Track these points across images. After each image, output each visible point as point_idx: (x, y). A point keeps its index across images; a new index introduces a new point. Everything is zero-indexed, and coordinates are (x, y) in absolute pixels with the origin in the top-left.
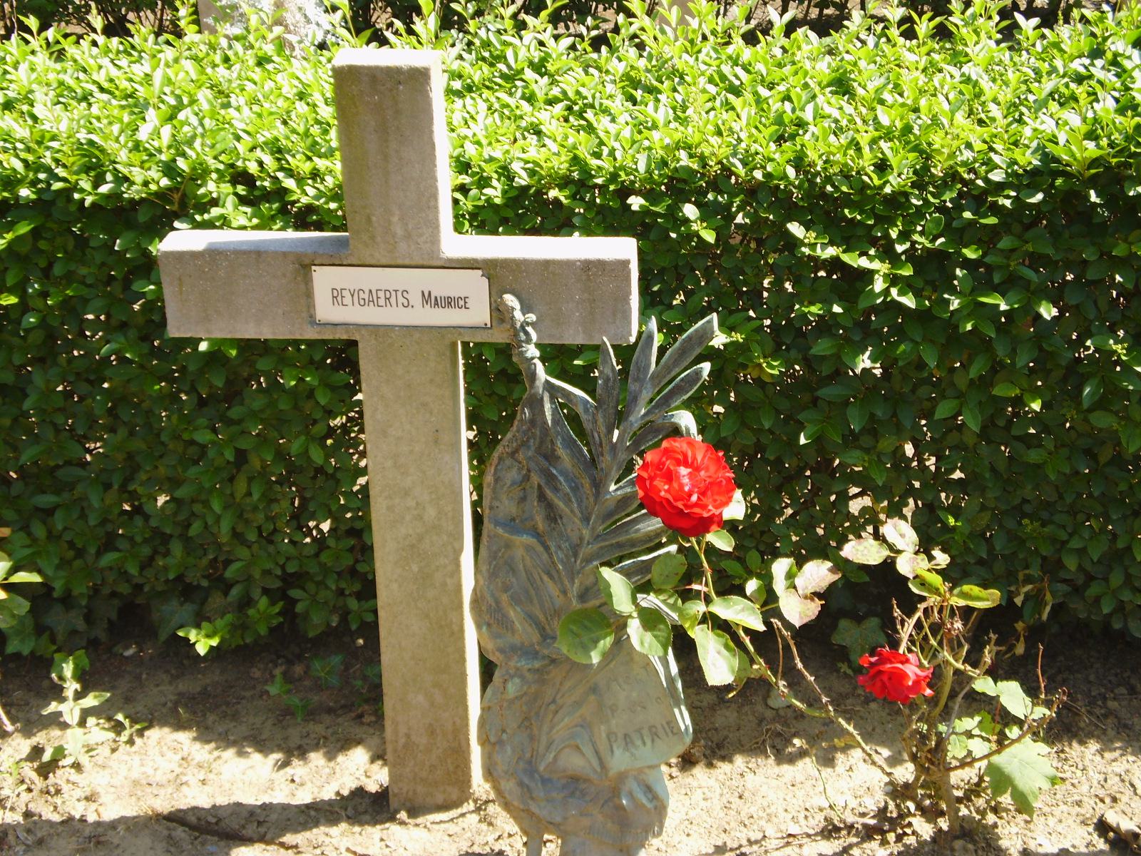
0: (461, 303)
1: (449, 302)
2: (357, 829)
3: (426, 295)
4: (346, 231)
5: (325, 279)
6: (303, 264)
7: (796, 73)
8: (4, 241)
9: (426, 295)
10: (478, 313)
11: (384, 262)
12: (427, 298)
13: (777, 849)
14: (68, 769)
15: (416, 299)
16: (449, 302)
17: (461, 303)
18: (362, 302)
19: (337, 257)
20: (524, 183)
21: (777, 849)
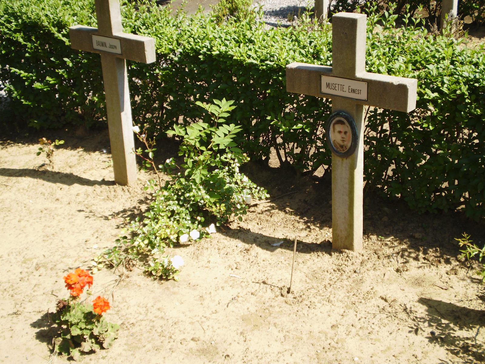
1: (353, 91)
15: (346, 88)
16: (353, 91)
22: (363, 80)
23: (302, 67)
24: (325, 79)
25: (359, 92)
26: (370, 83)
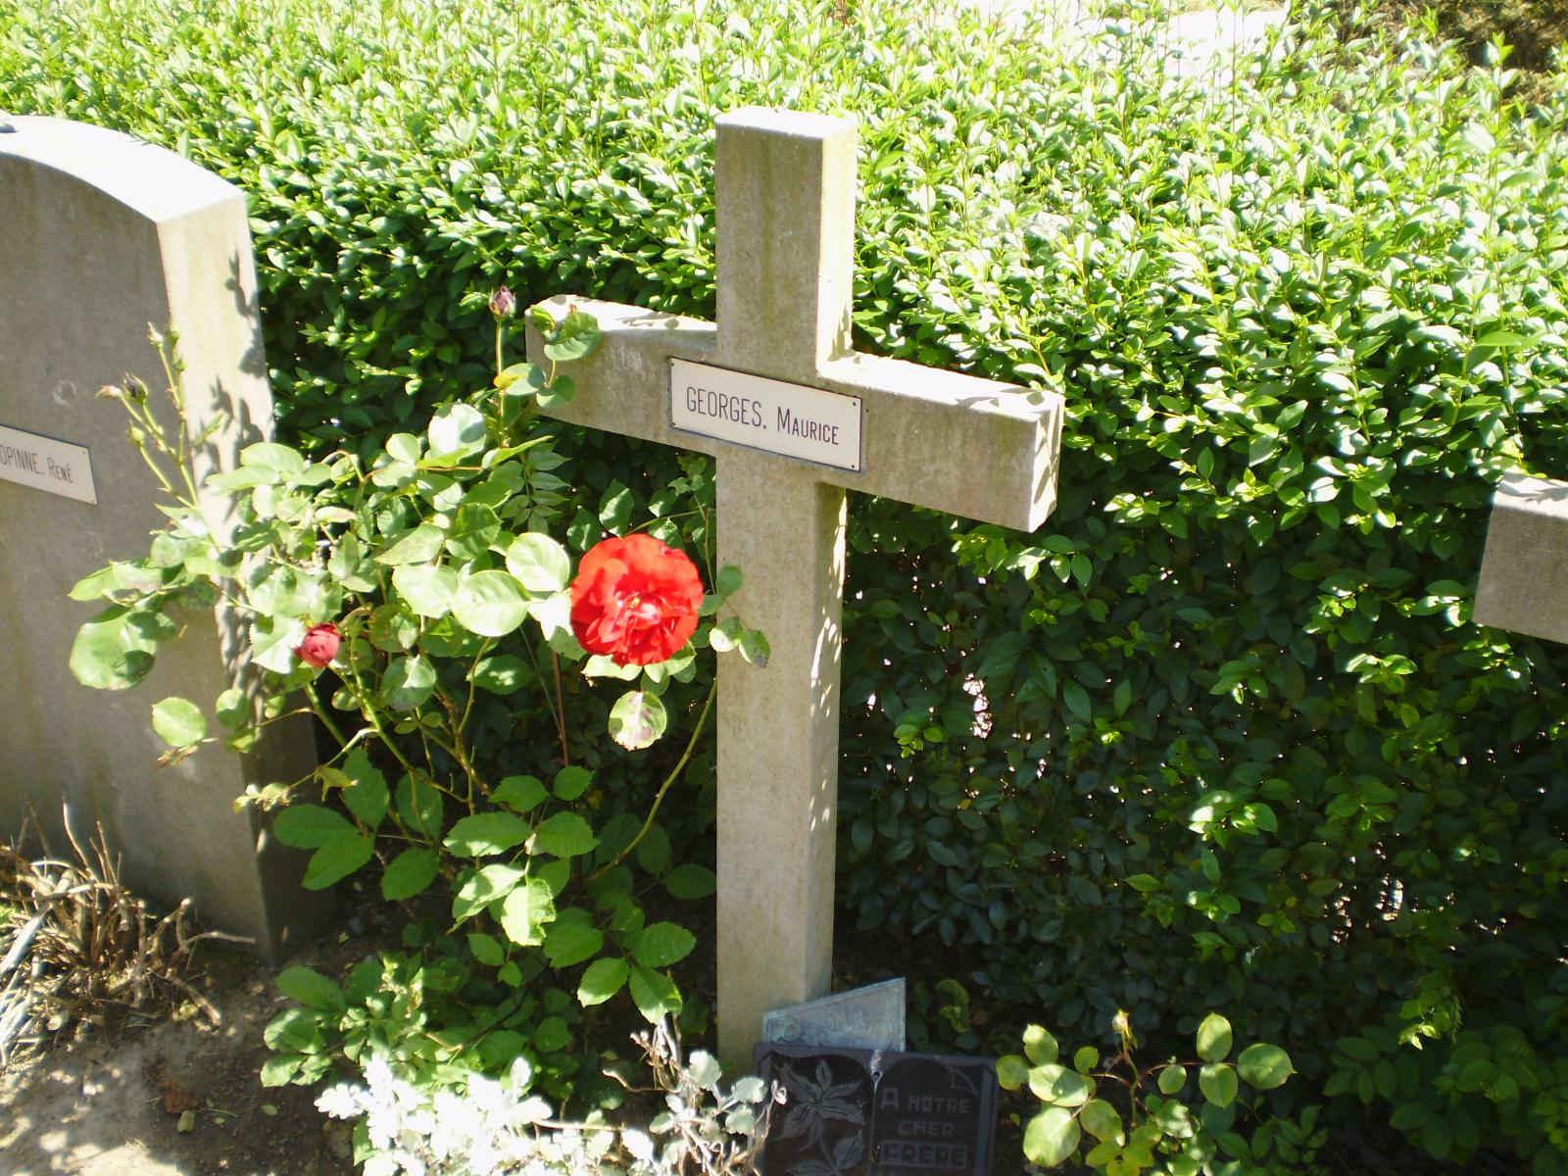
0: (829, 434)
1: (813, 430)
2: (809, 733)
3: (784, 414)
4: (712, 317)
5: (685, 375)
6: (664, 353)
7: (977, 190)
8: (1251, 464)
9: (784, 414)
10: (846, 453)
11: (730, 364)
12: (784, 418)
13: (423, 563)
14: (1008, 839)
15: (770, 418)
16: (813, 430)
17: (829, 434)
18: (735, 417)
19: (700, 351)
20: (1493, 459)
21: (423, 563)
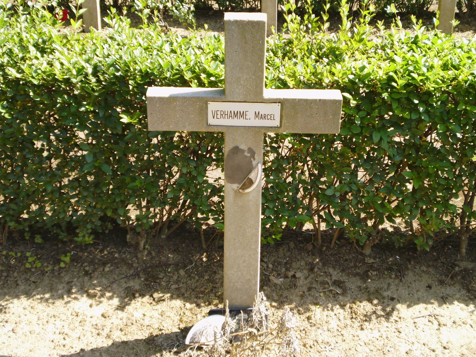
1: (263, 117)
15: (251, 115)
16: (263, 117)
17: (269, 117)
22: (274, 101)
23: (188, 94)
24: (212, 106)
25: (271, 117)
26: (282, 102)
